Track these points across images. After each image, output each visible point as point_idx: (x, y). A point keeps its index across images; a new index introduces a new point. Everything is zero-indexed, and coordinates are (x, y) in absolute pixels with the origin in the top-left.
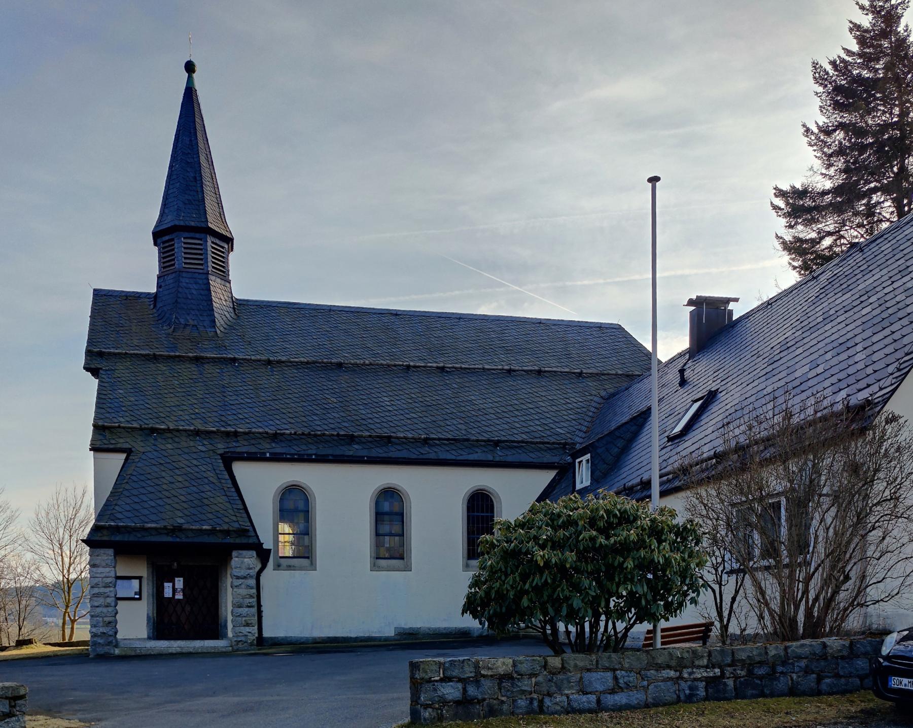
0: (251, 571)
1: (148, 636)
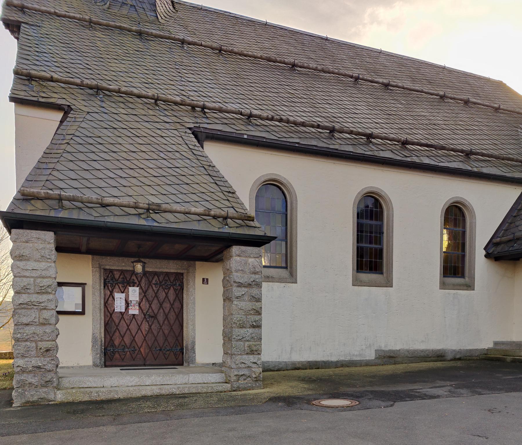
0: (257, 276)
1: (94, 362)
